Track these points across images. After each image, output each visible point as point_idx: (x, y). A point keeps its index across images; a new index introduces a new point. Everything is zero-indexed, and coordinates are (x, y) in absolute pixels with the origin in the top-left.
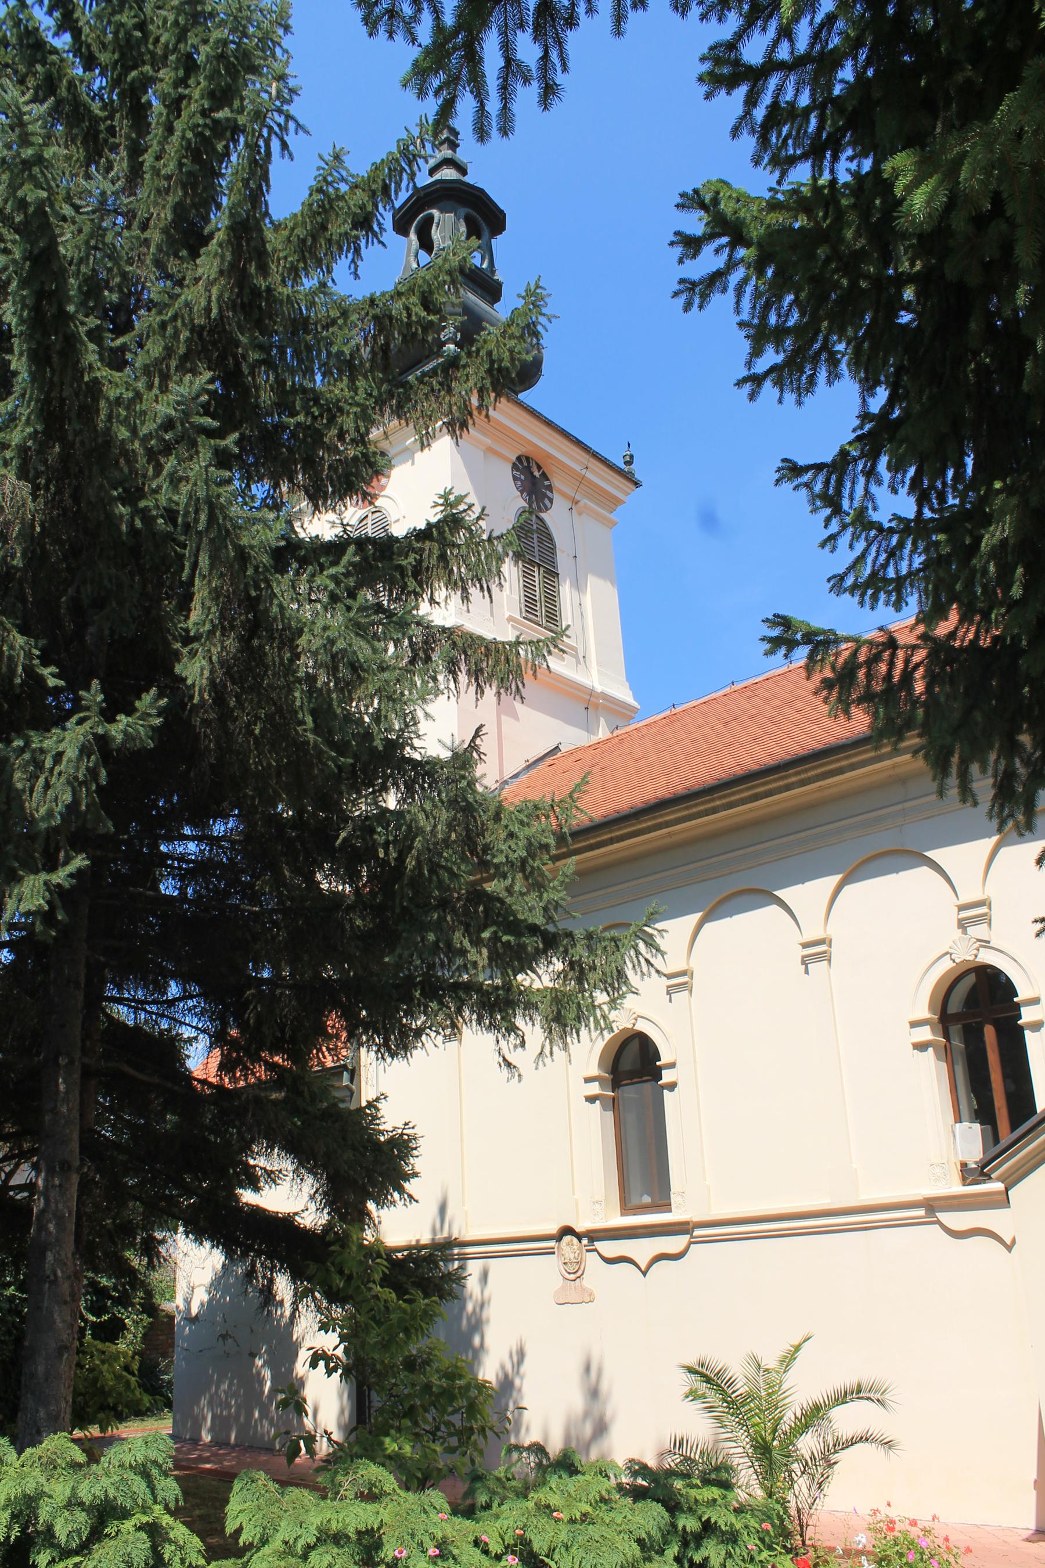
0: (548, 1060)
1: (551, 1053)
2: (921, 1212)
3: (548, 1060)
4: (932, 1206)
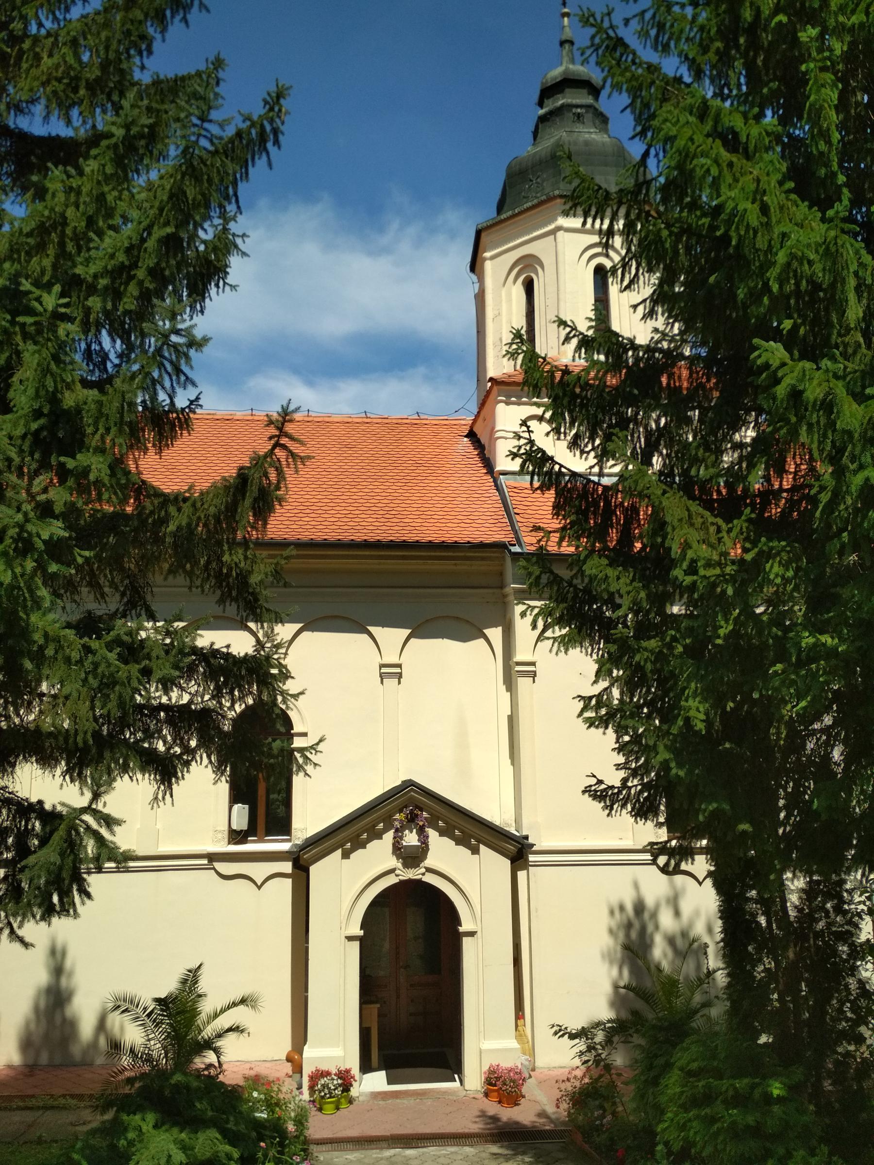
0: (161, 804)
1: (164, 798)
2: (205, 862)
3: (161, 804)
4: (212, 857)
